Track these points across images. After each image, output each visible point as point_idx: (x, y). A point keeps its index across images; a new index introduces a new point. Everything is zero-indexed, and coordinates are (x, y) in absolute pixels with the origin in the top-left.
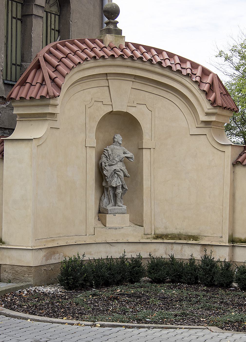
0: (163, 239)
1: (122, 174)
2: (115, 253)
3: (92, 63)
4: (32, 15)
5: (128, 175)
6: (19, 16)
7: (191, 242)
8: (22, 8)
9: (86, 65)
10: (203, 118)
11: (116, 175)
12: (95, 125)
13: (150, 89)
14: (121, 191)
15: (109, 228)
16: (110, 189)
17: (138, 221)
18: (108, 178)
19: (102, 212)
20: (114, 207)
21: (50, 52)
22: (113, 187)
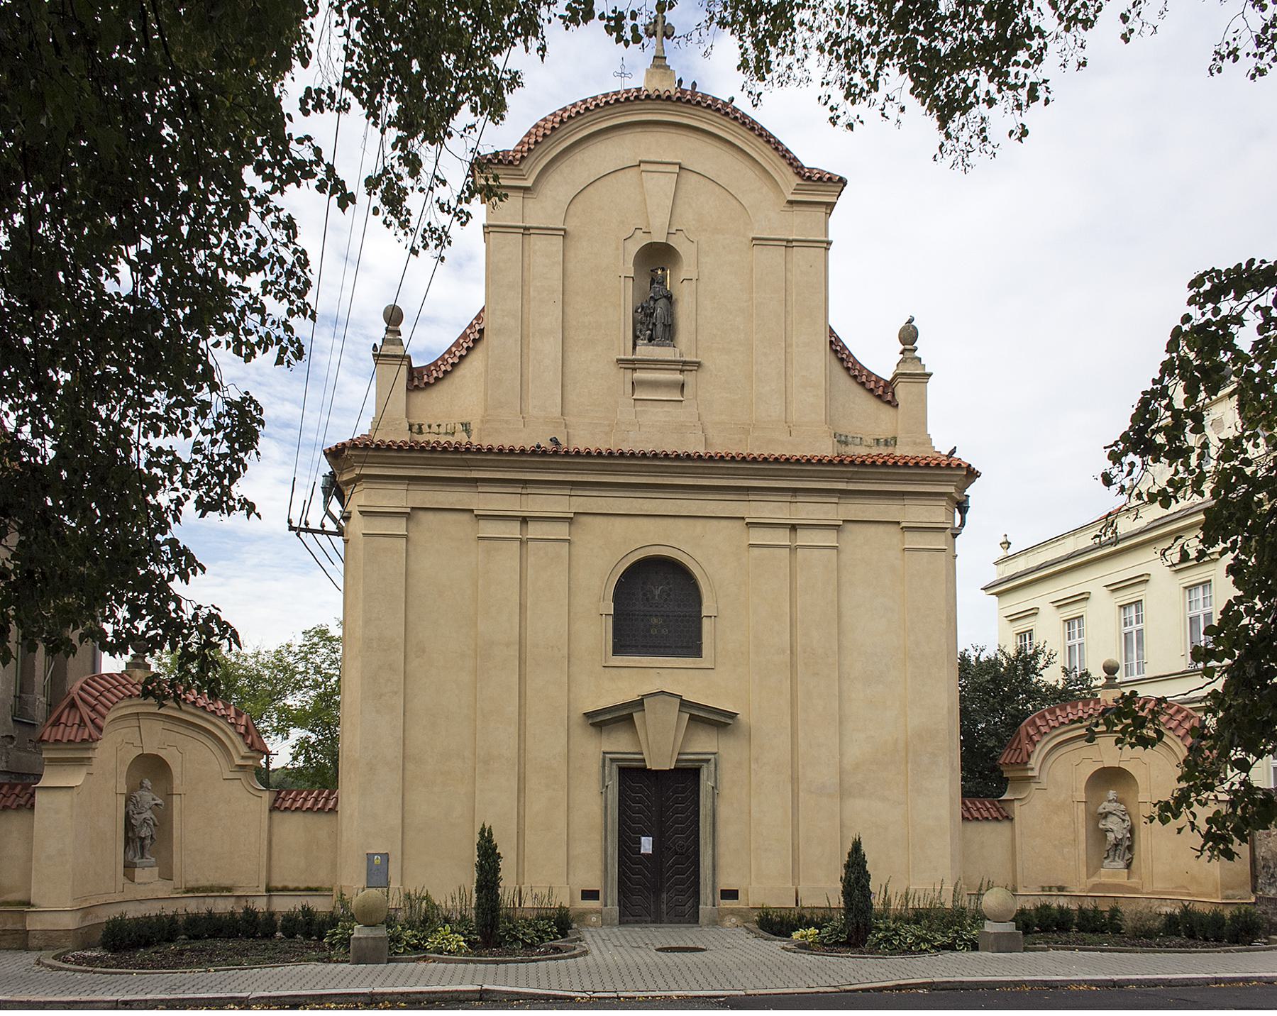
2: (152, 910)
3: (126, 702)
9: (122, 704)
10: (239, 762)
13: (182, 730)
17: (167, 875)
19: (129, 867)
21: (82, 689)
22: (143, 837)
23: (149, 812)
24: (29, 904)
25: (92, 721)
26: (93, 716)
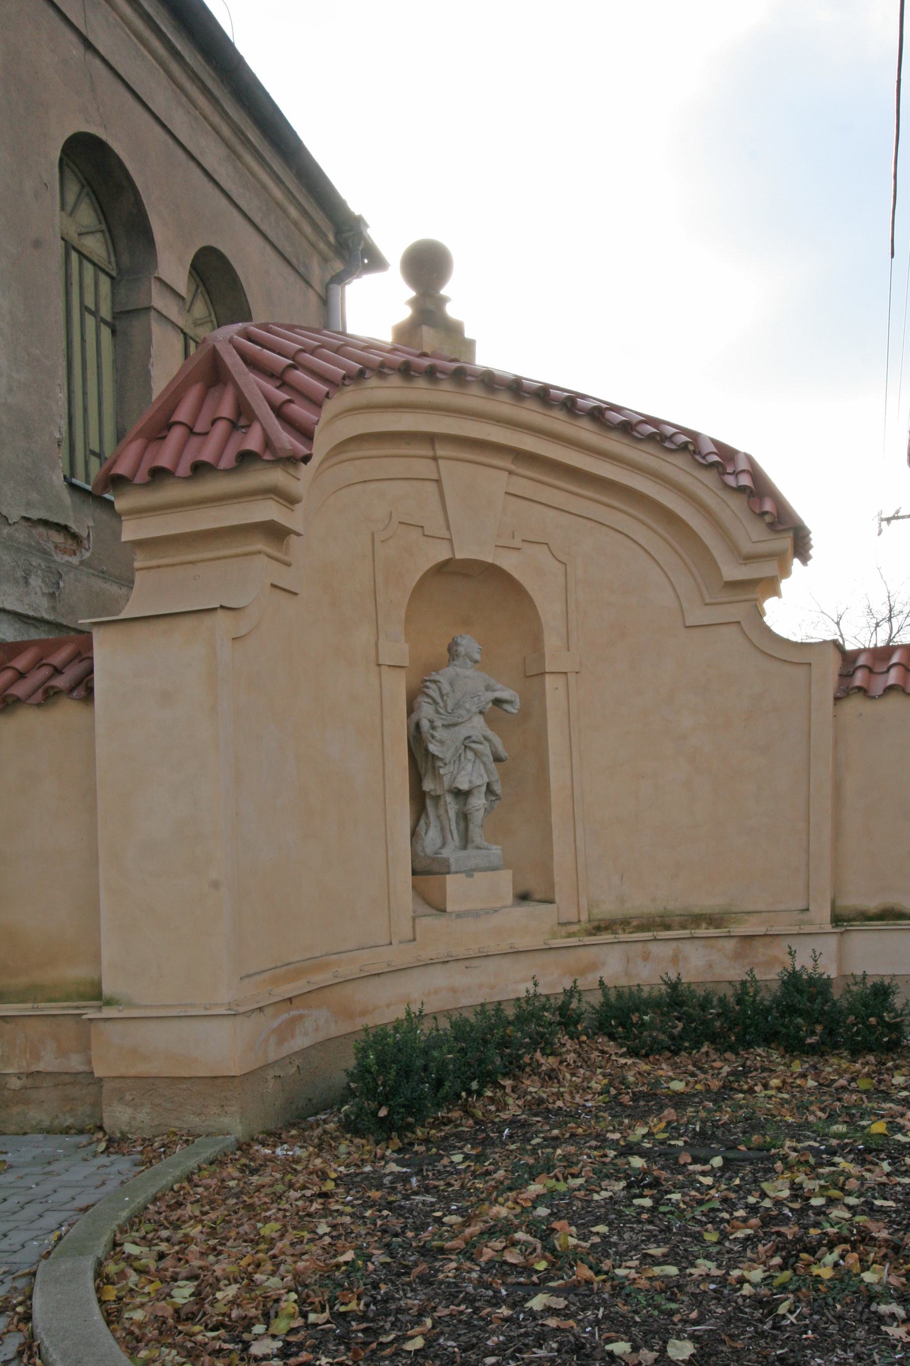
0: (614, 932)
1: (484, 749)
5: (503, 753)
6: (106, 312)
7: (702, 932)
11: (470, 755)
12: (402, 598)
14: (484, 801)
15: (459, 915)
16: (449, 798)
18: (445, 764)
19: (426, 871)
20: (463, 853)
23: (479, 721)
24: (94, 993)
25: (279, 411)
26: (282, 396)
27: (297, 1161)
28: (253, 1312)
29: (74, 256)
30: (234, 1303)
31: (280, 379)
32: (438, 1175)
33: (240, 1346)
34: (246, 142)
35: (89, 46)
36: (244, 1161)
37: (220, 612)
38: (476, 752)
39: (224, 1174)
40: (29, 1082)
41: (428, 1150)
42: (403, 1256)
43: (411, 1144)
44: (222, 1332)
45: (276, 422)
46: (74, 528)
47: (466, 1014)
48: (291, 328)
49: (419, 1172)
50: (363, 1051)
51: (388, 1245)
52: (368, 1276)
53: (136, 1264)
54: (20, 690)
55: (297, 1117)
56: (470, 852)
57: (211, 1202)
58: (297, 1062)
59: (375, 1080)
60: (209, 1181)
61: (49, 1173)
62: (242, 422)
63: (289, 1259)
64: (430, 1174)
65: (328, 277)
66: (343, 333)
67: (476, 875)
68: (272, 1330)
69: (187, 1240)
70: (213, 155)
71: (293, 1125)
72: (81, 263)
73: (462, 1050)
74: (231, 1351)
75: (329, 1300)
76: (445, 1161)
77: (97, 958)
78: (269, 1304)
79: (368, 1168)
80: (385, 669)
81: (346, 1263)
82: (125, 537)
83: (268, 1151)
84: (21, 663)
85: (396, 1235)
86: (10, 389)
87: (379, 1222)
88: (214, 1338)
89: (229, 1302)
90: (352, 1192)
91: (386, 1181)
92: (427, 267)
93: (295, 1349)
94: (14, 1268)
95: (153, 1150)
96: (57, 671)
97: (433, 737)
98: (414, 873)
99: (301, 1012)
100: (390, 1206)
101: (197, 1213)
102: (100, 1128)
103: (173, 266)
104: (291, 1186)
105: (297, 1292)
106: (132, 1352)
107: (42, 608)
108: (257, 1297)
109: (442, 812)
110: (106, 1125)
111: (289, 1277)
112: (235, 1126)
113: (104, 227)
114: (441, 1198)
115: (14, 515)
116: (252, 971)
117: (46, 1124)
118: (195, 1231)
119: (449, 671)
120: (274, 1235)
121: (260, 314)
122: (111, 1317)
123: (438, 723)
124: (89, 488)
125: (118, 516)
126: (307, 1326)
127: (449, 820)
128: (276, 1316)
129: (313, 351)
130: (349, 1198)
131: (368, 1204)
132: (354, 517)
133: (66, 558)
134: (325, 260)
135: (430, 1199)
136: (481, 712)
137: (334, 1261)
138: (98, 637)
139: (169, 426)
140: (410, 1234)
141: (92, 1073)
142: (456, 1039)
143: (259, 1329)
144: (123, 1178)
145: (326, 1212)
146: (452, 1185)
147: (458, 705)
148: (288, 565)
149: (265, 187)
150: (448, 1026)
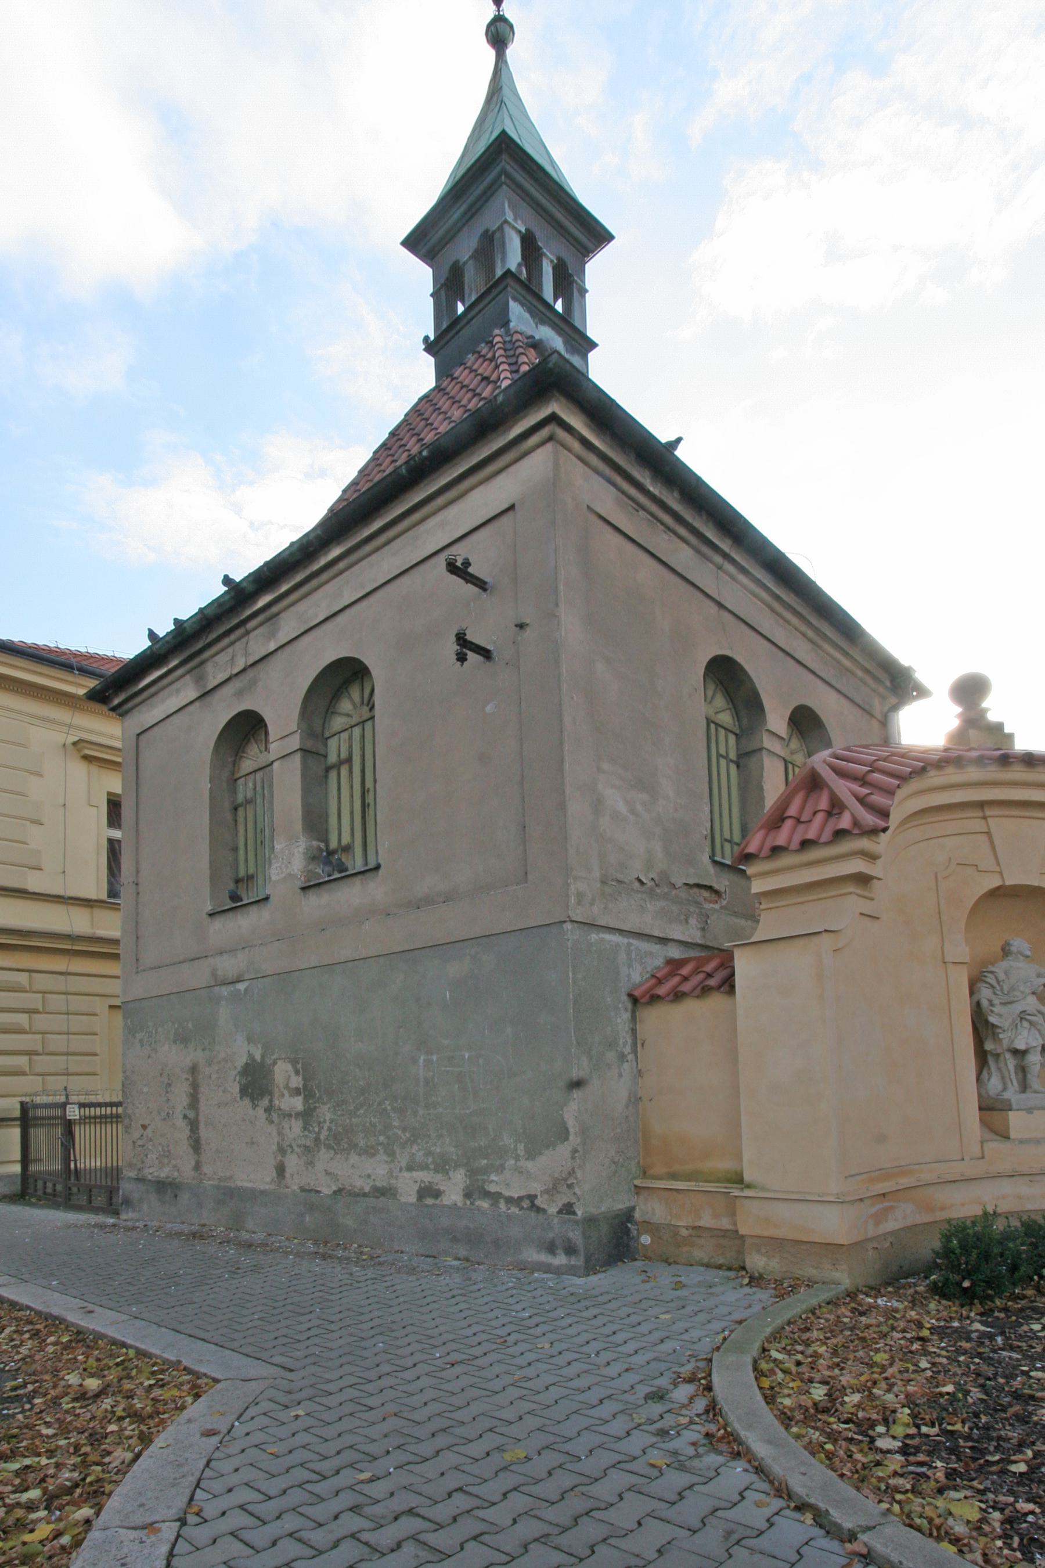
4: (761, 749)
6: (733, 755)
8: (737, 744)
16: (1008, 1056)
19: (991, 1108)
20: (1023, 1096)
24: (738, 1179)
25: (862, 800)
26: (865, 791)
27: (896, 1310)
28: (875, 1416)
29: (712, 726)
30: (858, 1406)
31: (863, 781)
32: (1020, 1338)
33: (868, 1439)
34: (825, 637)
35: (720, 605)
36: (853, 1305)
37: (825, 935)
38: (1031, 1023)
39: (839, 1312)
40: (693, 1233)
41: (1009, 1317)
42: (997, 1396)
43: (992, 1311)
44: (851, 1425)
45: (862, 809)
46: (716, 886)
47: (1033, 1217)
48: (866, 747)
49: (1003, 1333)
50: (947, 1238)
51: (983, 1386)
52: (969, 1407)
53: (781, 1366)
54: (686, 987)
55: (894, 1278)
56: (1029, 1095)
57: (832, 1331)
58: (890, 1239)
59: (958, 1260)
60: (828, 1316)
61: (711, 1294)
62: (835, 812)
63: (900, 1383)
64: (1013, 1336)
65: (886, 708)
66: (900, 744)
67: (1035, 1112)
68: (891, 1432)
69: (816, 1355)
70: (802, 649)
71: (889, 1284)
72: (717, 730)
73: (1032, 1244)
74: (861, 1441)
75: (937, 1419)
76: (1025, 1328)
77: (739, 1156)
78: (888, 1413)
79: (956, 1324)
80: (949, 966)
81: (948, 1394)
82: (753, 891)
83: (871, 1301)
84: (685, 971)
85: (989, 1379)
86: (676, 810)
87: (972, 1367)
88: (846, 1429)
89: (855, 1406)
90: (945, 1340)
91: (974, 1335)
92: (970, 691)
93: (912, 1450)
94: (696, 1353)
95: (785, 1288)
96: (709, 975)
97: (992, 1011)
98: (980, 1109)
99: (892, 1204)
100: (980, 1355)
101: (822, 1337)
102: (743, 1268)
103: (777, 720)
104: (893, 1328)
105: (909, 1408)
106: (787, 1427)
107: (696, 937)
108: (877, 1406)
109: (1002, 1065)
110: (748, 1266)
111: (902, 1396)
112: (843, 1278)
113: (731, 706)
114: (1026, 1356)
115: (679, 884)
116: (853, 1173)
117: (706, 1260)
118: (822, 1350)
119: (1004, 964)
120: (884, 1362)
121: (839, 743)
122: (770, 1399)
123: (996, 1002)
124: (728, 862)
125: (749, 878)
126: (920, 1435)
127: (1009, 1071)
128: (894, 1422)
129: (884, 760)
130: (943, 1345)
131: (960, 1351)
132: (916, 864)
133: (711, 905)
134: (883, 698)
135: (1015, 1355)
136: (1033, 993)
137: (938, 1390)
138: (738, 954)
139: (783, 819)
140: (1001, 1380)
141: (737, 1231)
142: (1026, 1234)
143: (881, 1429)
144: (764, 1305)
145: (925, 1353)
146: (1034, 1348)
147: (1012, 989)
148: (872, 899)
149: (838, 662)
150: (1019, 1224)
